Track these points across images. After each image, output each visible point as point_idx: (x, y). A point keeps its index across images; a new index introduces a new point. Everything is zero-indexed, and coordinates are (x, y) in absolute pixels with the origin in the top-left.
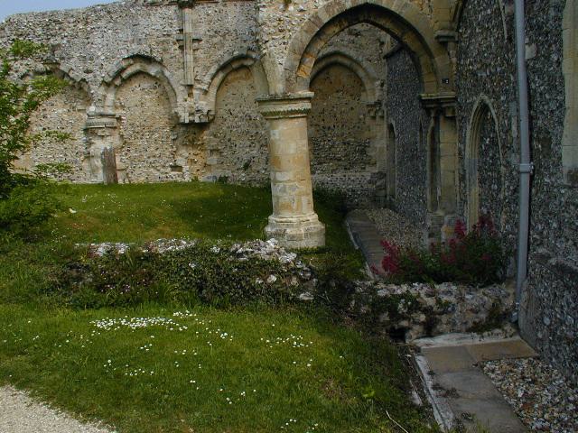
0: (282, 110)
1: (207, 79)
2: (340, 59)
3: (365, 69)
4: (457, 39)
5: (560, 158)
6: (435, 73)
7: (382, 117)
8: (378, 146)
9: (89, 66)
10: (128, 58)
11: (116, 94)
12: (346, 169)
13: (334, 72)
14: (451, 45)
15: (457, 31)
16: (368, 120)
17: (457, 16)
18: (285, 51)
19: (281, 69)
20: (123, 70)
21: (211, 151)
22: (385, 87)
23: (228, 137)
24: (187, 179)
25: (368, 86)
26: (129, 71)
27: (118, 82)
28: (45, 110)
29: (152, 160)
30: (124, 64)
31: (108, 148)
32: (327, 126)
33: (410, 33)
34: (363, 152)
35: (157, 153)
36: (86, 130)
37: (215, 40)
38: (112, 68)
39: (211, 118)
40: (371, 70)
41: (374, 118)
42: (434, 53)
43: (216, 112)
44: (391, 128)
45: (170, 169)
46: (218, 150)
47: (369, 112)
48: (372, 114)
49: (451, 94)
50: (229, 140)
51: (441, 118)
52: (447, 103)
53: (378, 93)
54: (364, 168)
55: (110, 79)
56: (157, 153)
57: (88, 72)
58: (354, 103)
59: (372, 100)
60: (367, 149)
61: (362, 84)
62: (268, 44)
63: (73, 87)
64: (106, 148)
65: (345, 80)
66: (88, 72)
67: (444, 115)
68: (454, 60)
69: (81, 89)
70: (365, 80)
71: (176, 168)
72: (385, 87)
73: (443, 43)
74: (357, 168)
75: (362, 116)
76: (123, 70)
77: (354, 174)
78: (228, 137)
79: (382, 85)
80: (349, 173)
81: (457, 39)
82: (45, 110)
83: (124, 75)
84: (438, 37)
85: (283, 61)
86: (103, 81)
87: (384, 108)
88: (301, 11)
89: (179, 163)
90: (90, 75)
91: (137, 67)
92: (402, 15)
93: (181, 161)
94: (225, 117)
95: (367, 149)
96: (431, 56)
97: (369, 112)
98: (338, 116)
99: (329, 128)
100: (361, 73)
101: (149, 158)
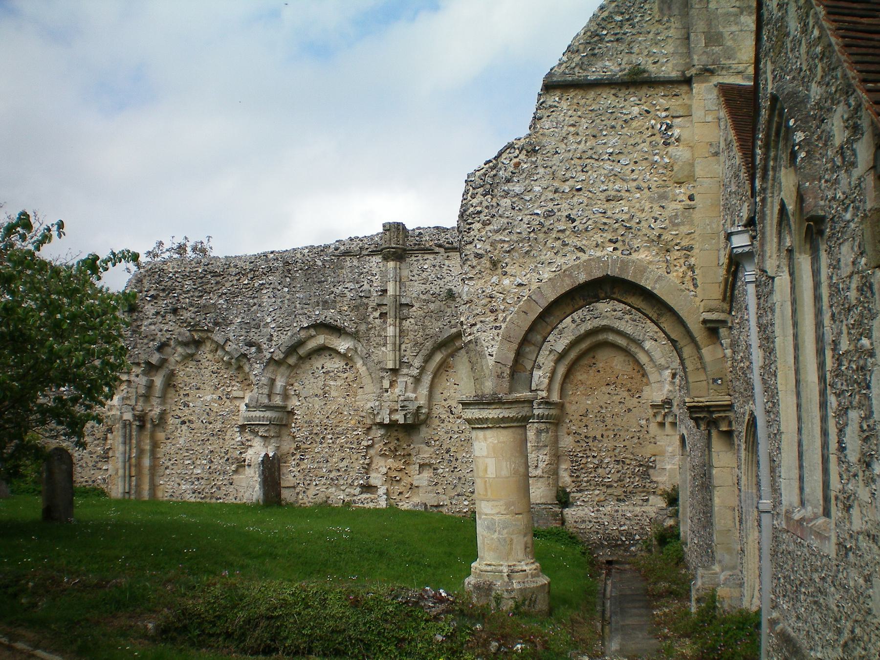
0: (491, 416)
1: (417, 363)
2: (611, 337)
3: (647, 352)
4: (730, 325)
5: (781, 494)
6: (704, 368)
7: (674, 424)
8: (668, 467)
9: (253, 336)
10: (308, 328)
11: (289, 377)
12: (619, 500)
13: (604, 358)
14: (723, 332)
15: (730, 313)
16: (653, 428)
17: (728, 294)
18: (496, 338)
19: (491, 361)
20: (301, 343)
21: (421, 466)
22: (677, 381)
23: (445, 447)
24: (383, 504)
25: (653, 376)
26: (312, 344)
27: (292, 361)
28: (187, 395)
29: (334, 474)
30: (303, 334)
31: (271, 455)
32: (592, 434)
33: (669, 314)
34: (645, 475)
35: (342, 465)
36: (578, 134)
37: (432, 306)
38: (285, 339)
39: (422, 417)
40: (657, 355)
41: (662, 425)
42: (700, 343)
43: (430, 409)
44: (683, 439)
45: (358, 489)
46: (430, 465)
47: (655, 416)
48: (659, 419)
49: (725, 400)
50: (448, 451)
51: (714, 433)
52: (719, 411)
53: (667, 387)
54: (647, 500)
55: (282, 356)
56: (342, 465)
57: (250, 344)
58: (632, 402)
59: (658, 397)
60: (651, 471)
61: (644, 375)
62: (475, 329)
63: (229, 364)
64: (267, 455)
65: (619, 367)
66: (250, 344)
67: (717, 427)
68: (728, 352)
69: (240, 368)
70: (648, 368)
71: (368, 488)
72: (677, 381)
73: (713, 329)
74: (637, 499)
75: (643, 422)
76: (301, 343)
77: (631, 508)
78: (445, 447)
79: (674, 376)
80: (623, 507)
81: (730, 325)
82: (187, 395)
83: (302, 351)
84: (705, 322)
85: (494, 350)
86: (271, 358)
87: (675, 409)
88: (520, 285)
89: (373, 482)
90: (253, 349)
91: (321, 339)
92: (655, 291)
93: (376, 479)
94: (443, 416)
95: (651, 471)
96: (698, 348)
97: (655, 416)
98: (608, 421)
99: (595, 438)
100: (643, 358)
101: (330, 471)
